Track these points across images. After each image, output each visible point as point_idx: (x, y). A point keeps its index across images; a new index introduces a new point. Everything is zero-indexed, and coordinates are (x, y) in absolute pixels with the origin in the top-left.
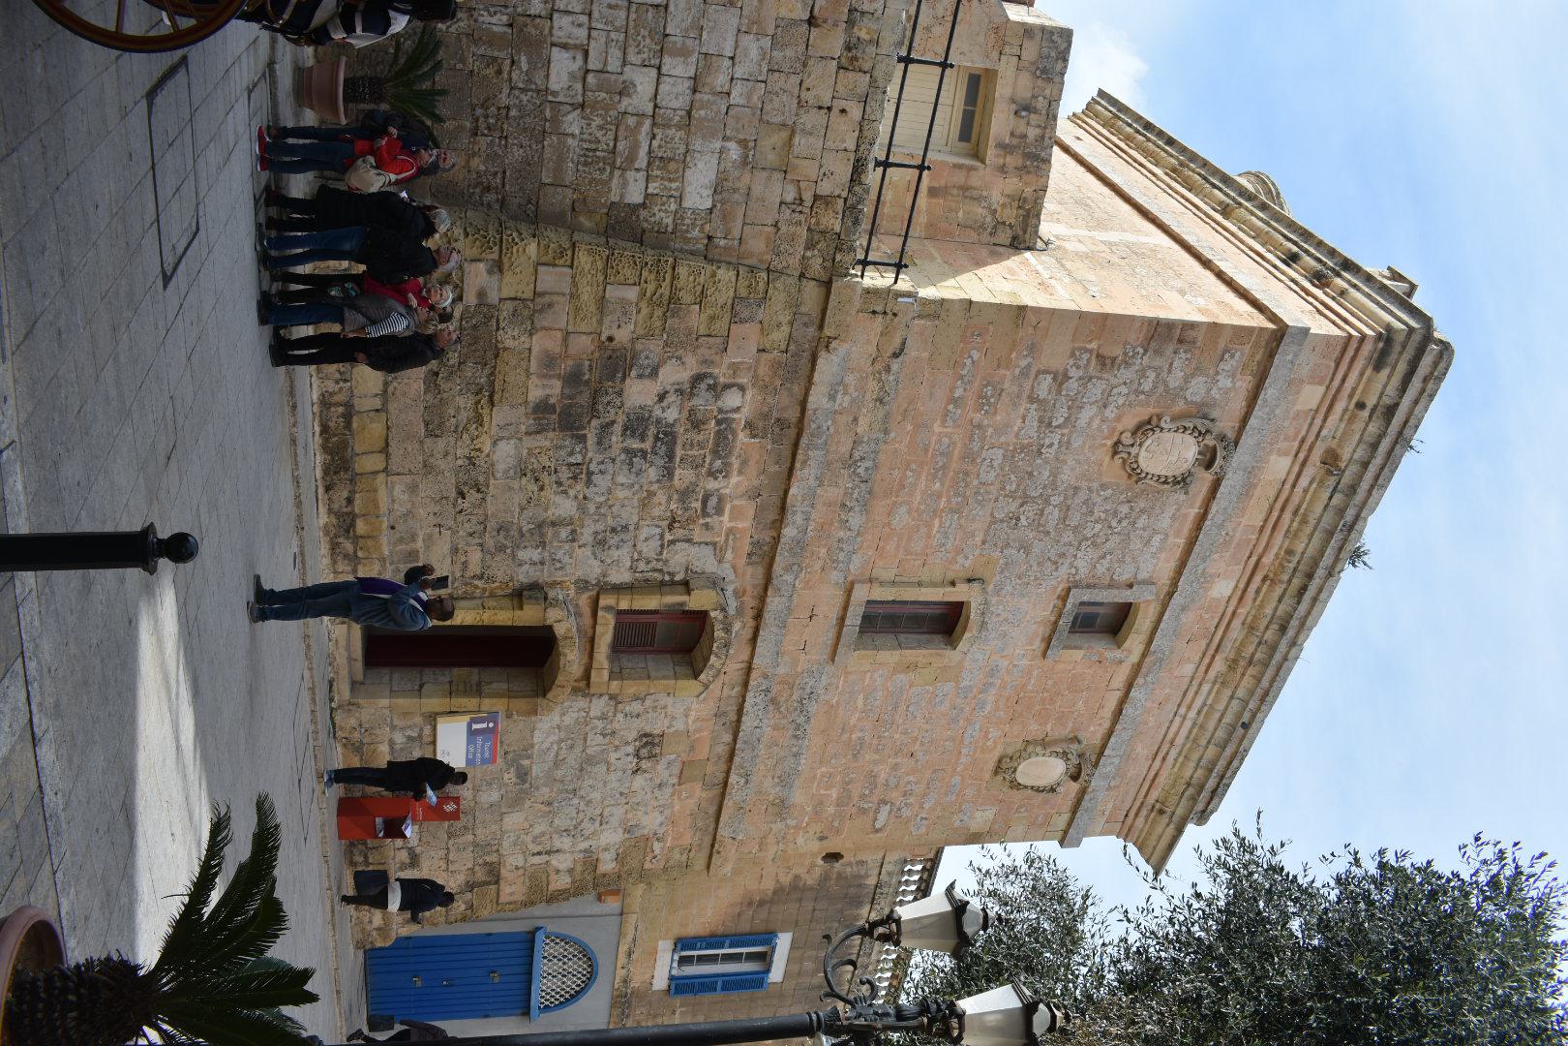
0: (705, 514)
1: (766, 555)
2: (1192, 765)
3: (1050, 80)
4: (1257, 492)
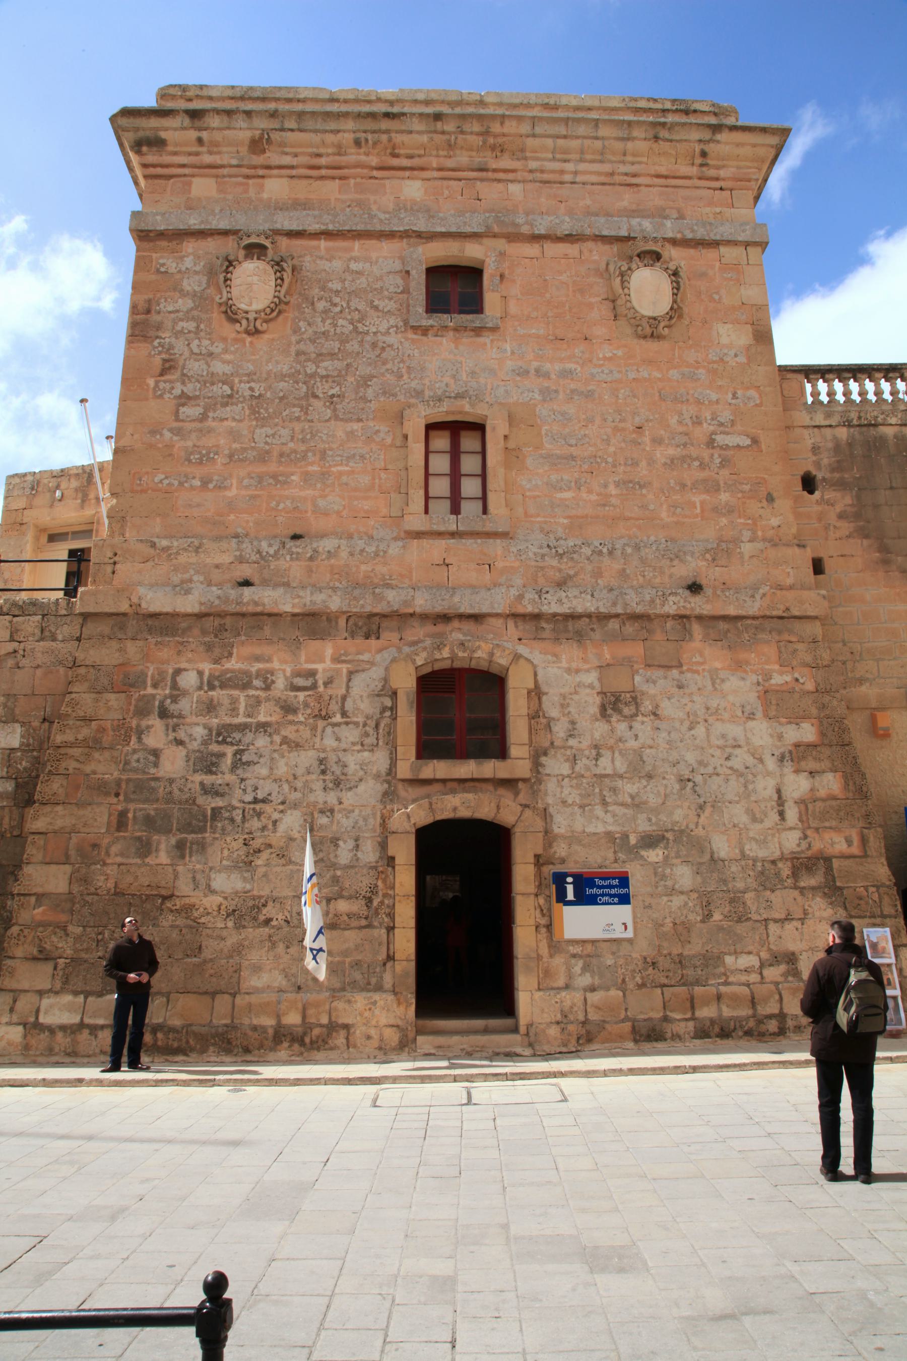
0: (314, 686)
1: (370, 625)
2: (630, 145)
3: (38, 483)
4: (302, 196)
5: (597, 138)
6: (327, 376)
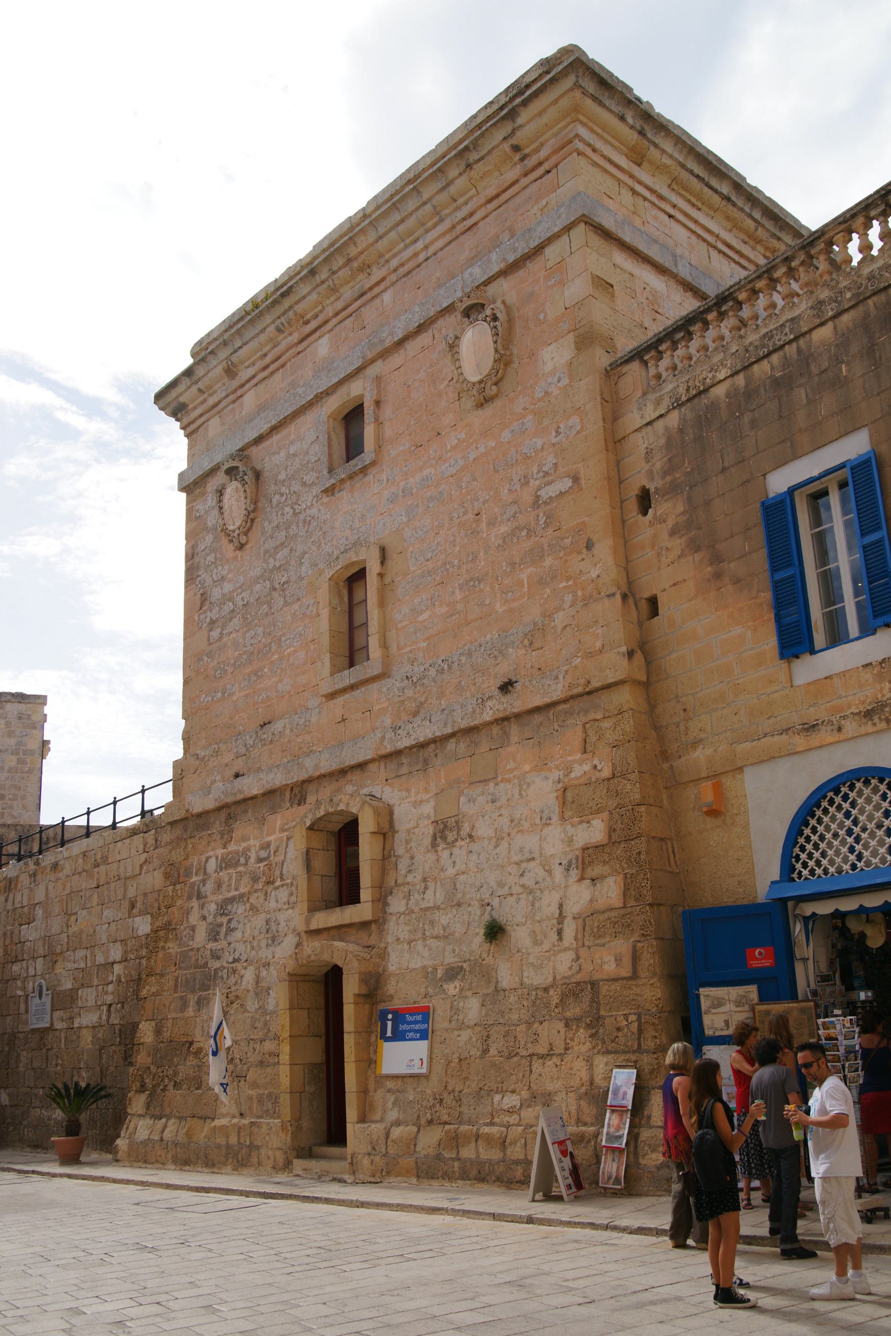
2: (452, 189)
5: (425, 203)
6: (280, 567)
